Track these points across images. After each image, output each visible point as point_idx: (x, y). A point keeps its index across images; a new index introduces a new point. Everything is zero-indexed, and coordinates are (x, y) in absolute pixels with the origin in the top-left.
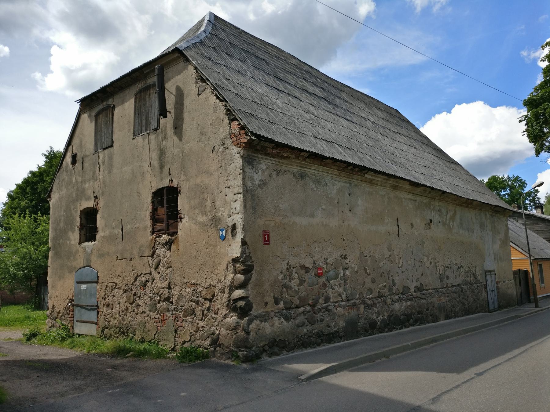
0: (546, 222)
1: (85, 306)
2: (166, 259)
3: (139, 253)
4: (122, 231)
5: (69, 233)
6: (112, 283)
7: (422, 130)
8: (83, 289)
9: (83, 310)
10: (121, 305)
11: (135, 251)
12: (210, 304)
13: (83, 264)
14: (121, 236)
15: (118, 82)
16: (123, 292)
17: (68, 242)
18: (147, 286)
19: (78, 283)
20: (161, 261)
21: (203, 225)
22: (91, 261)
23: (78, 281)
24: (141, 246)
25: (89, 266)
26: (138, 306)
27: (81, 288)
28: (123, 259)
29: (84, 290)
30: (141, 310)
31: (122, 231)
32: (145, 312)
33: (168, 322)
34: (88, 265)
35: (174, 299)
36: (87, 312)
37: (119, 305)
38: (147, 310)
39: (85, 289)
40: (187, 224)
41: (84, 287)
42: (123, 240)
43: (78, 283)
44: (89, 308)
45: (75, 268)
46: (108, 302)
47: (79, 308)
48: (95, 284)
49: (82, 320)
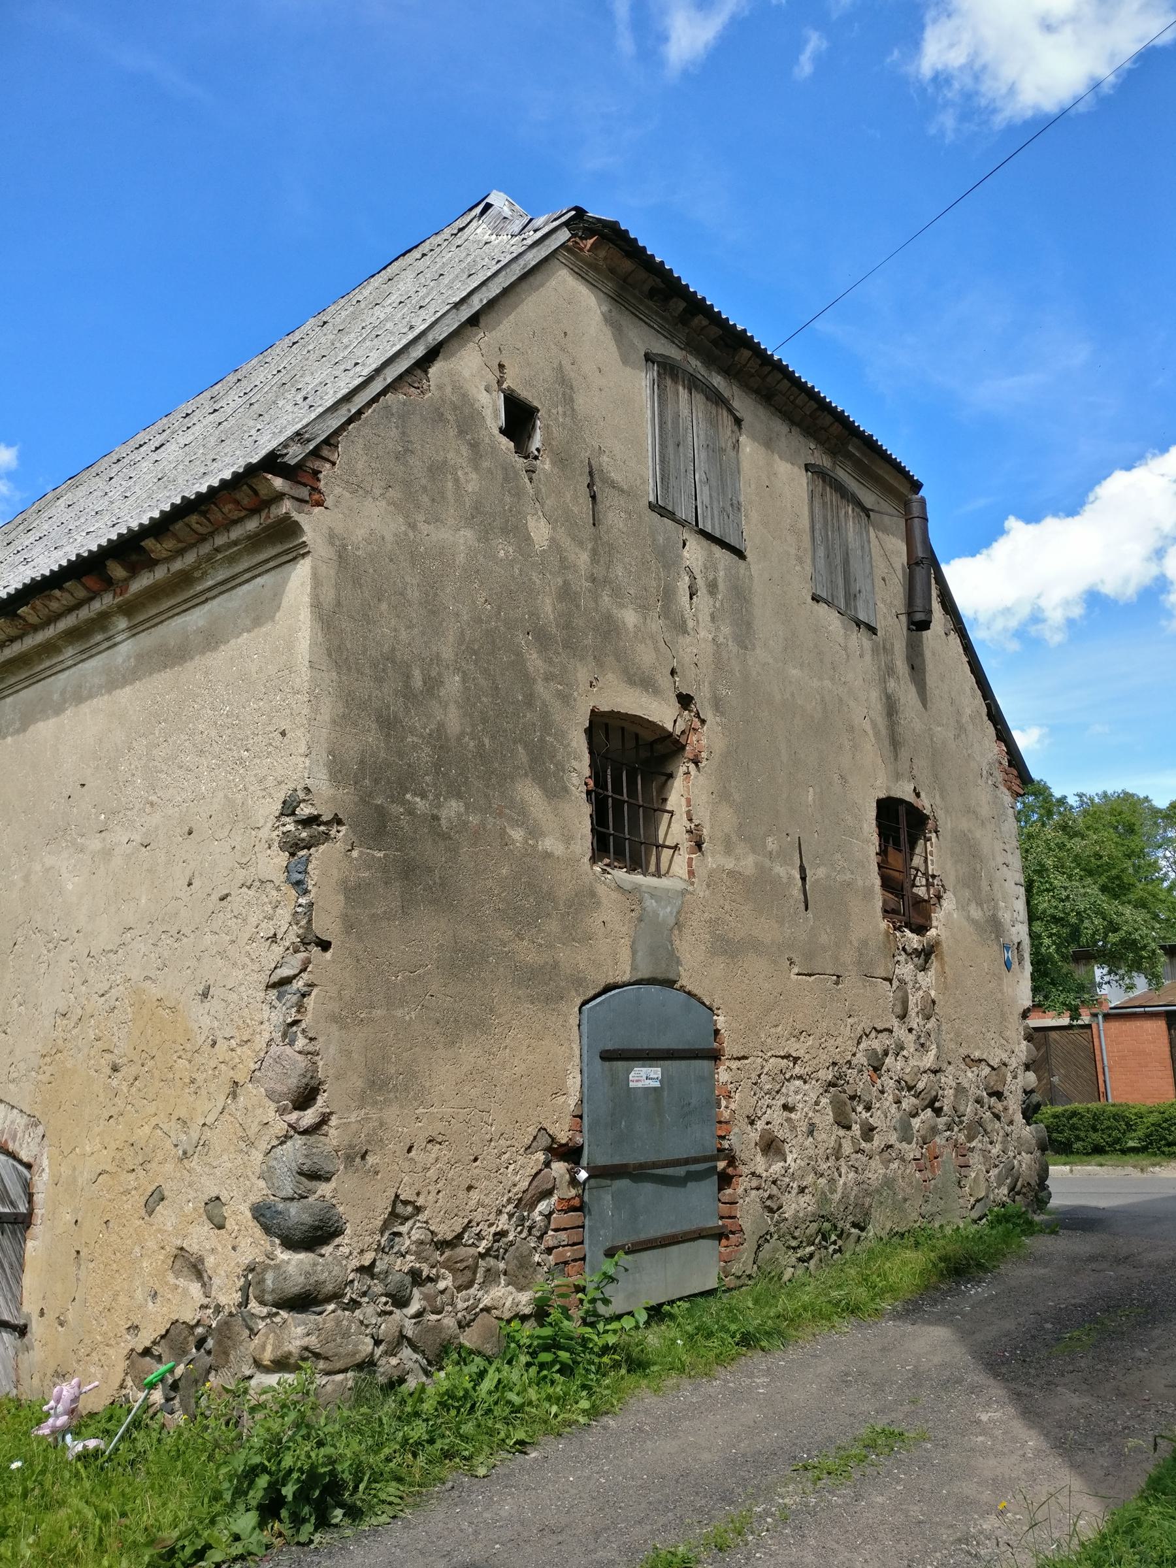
0: (149, 543)
1: (655, 1165)
2: (921, 993)
3: (859, 963)
4: (803, 879)
5: (519, 787)
6: (783, 1057)
7: (946, 569)
8: (640, 1085)
9: (648, 1188)
10: (821, 1136)
11: (848, 956)
12: (373, 1349)
13: (634, 968)
14: (796, 892)
15: (786, 383)
16: (821, 1091)
17: (517, 834)
18: (884, 1068)
19: (608, 1056)
20: (910, 997)
21: (974, 922)
22: (678, 962)
23: (609, 1047)
24: (864, 943)
25: (669, 983)
26: (868, 1132)
27: (632, 1085)
28: (810, 975)
29: (647, 1090)
30: (878, 1141)
31: (803, 879)
32: (891, 1146)
33: (943, 1161)
34: (659, 975)
35: (946, 1105)
36: (668, 1192)
37: (811, 1139)
38: (893, 1138)
39: (657, 1084)
40: (955, 916)
41: (645, 1076)
42: (807, 909)
43: (608, 1056)
44: (681, 1171)
45: (578, 982)
46: (770, 1132)
47: (623, 1184)
48: (706, 1064)
49: (643, 1236)
